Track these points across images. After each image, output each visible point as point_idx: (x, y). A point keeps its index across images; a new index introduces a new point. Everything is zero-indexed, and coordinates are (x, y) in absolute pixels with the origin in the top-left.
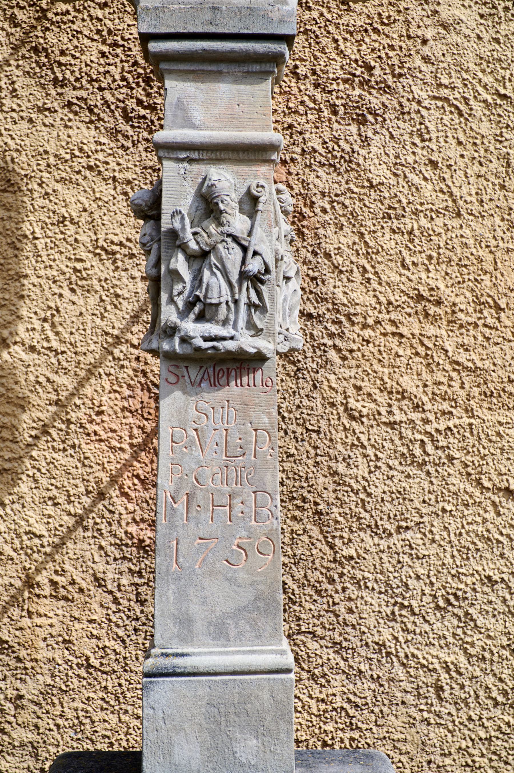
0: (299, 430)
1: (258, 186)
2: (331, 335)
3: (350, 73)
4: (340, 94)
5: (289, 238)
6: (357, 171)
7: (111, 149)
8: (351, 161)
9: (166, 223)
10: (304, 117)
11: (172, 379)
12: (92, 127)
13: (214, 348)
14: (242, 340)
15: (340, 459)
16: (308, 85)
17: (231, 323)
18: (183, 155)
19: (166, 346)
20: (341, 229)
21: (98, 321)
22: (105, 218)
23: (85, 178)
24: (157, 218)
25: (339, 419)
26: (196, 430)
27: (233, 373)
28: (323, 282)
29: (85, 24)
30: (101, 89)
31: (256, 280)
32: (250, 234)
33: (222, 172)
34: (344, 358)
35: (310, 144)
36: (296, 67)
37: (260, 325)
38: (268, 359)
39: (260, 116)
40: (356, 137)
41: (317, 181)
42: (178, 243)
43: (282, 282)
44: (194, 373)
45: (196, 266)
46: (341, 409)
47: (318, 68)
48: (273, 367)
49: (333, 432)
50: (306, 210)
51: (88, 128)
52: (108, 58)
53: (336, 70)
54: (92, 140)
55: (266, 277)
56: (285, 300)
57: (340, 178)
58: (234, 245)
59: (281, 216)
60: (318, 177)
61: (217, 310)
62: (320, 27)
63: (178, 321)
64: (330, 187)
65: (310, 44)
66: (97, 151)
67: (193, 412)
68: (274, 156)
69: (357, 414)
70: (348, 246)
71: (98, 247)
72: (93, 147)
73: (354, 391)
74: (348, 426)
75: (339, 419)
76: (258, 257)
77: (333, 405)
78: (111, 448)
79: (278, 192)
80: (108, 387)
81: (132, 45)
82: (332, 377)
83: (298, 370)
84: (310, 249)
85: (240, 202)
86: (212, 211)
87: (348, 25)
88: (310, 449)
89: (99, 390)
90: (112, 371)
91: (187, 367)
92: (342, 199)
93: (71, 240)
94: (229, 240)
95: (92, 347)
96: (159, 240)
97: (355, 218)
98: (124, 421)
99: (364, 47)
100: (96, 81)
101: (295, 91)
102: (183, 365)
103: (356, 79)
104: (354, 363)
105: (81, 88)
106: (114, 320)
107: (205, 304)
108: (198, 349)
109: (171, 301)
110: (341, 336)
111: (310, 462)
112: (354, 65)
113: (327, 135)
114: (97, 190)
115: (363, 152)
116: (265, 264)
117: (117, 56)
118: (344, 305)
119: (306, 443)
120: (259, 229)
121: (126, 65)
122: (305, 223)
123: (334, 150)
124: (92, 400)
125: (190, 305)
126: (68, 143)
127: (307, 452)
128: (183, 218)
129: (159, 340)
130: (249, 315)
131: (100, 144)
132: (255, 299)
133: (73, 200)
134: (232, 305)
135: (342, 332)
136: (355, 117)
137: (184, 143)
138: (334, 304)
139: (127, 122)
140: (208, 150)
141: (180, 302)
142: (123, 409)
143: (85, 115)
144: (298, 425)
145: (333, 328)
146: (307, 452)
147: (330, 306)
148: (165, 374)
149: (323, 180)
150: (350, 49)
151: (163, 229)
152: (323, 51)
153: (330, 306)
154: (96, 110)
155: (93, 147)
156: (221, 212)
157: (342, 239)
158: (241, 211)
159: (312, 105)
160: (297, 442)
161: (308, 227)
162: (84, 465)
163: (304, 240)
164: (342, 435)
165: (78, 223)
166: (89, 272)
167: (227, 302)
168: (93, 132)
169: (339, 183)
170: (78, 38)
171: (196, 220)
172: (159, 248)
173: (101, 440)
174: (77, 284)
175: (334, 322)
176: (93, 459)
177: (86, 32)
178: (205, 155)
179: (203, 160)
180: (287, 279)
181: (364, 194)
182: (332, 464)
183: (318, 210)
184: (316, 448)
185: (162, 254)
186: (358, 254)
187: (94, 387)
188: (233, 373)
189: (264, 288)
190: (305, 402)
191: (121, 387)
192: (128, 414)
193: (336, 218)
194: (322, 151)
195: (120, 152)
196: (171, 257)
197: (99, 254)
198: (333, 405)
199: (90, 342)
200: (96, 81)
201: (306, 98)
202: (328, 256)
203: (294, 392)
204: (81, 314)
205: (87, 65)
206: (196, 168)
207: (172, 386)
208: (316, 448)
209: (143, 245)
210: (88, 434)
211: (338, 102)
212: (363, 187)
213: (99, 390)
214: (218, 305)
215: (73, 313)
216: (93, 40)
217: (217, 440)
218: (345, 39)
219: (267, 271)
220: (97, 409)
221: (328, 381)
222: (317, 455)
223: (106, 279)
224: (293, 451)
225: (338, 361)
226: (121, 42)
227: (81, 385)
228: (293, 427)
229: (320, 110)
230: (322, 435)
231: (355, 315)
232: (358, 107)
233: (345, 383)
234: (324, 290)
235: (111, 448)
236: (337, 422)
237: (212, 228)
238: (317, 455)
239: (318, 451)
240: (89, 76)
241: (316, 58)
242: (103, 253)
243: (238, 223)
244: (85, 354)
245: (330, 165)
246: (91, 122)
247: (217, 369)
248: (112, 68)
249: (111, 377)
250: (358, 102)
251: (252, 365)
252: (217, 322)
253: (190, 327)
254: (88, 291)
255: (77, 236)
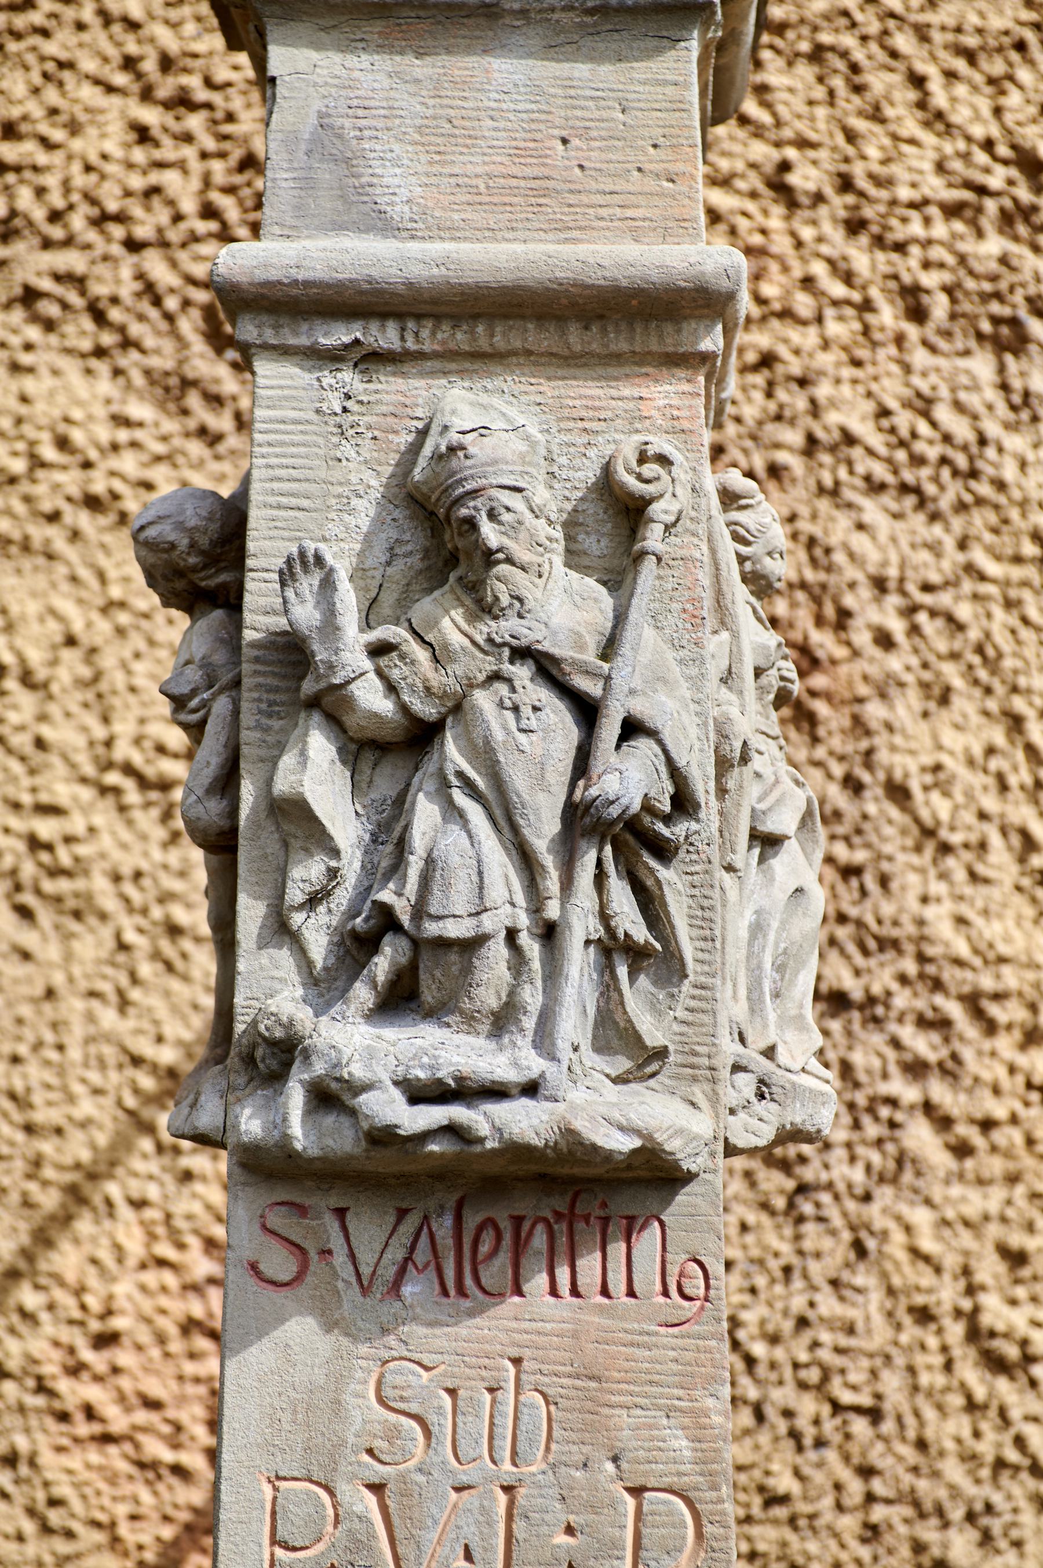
0: (808, 1406)
1: (642, 459)
2: (916, 1069)
3: (968, 185)
4: (937, 253)
5: (771, 679)
6: (997, 507)
7: (164, 439)
8: (974, 474)
9: (262, 609)
10: (813, 331)
11: (279, 1263)
12: (102, 367)
13: (452, 1130)
14: (577, 1095)
15: (957, 1514)
16: (825, 228)
17: (529, 1023)
18: (338, 335)
19: (251, 1124)
20: (945, 699)
21: (108, 1017)
22: (138, 667)
23: (75, 535)
24: (230, 599)
25: (948, 1366)
26: (377, 1488)
27: (539, 1240)
28: (884, 881)
29: (85, 37)
30: (133, 245)
31: (637, 842)
32: (609, 649)
33: (496, 401)
34: (962, 1150)
35: (833, 418)
36: (785, 166)
37: (653, 1035)
38: (690, 1177)
39: (651, 184)
40: (991, 394)
41: (860, 542)
42: (309, 687)
43: (745, 856)
44: (372, 1236)
45: (385, 786)
46: (956, 1331)
47: (858, 170)
48: (711, 1215)
49: (930, 1414)
50: (823, 641)
51: (89, 371)
52: (157, 144)
53: (918, 174)
54: (100, 411)
55: (679, 830)
56: (757, 929)
57: (937, 530)
58: (543, 694)
59: (740, 594)
60: (861, 527)
61: (468, 970)
62: (864, 39)
63: (303, 1016)
64: (903, 565)
65: (831, 93)
66: (115, 447)
67: (364, 1409)
68: (712, 341)
69: (1012, 1352)
70: (971, 762)
71: (108, 766)
72: (104, 433)
73: (1001, 1267)
74: (980, 1393)
75: (948, 1366)
76: (644, 745)
77: (924, 1315)
78: (141, 1465)
79: (729, 498)
80: (135, 1246)
81: (237, 104)
82: (921, 1217)
83: (802, 1189)
84: (838, 770)
85: (571, 526)
86: (452, 560)
87: (959, 30)
88: (846, 1475)
89: (105, 1255)
90: (153, 1192)
91: (341, 1213)
92: (944, 599)
93: (22, 741)
94: (522, 673)
95: (86, 1107)
96: (236, 683)
97: (993, 664)
98: (190, 1368)
99: (1013, 99)
100: (120, 218)
101: (782, 244)
102: (323, 1202)
103: (991, 205)
104: (996, 1166)
105: (69, 242)
106: (162, 1010)
107: (416, 943)
108: (383, 1137)
109: (281, 929)
110: (950, 1070)
111: (849, 1524)
112: (981, 157)
113: (892, 390)
114: (112, 574)
115: (1017, 443)
116: (675, 772)
117: (188, 138)
118: (959, 962)
119: (831, 1456)
120: (649, 633)
121: (217, 167)
122: (819, 681)
123: (914, 435)
124: (79, 1291)
125: (357, 946)
126: (19, 421)
127: (838, 1487)
128: (328, 584)
129: (229, 1096)
130: (609, 988)
131: (121, 421)
132: (630, 922)
133: (33, 608)
134: (532, 948)
135: (955, 1057)
136: (986, 327)
137: (340, 286)
138: (922, 958)
139: (219, 351)
140: (438, 318)
141: (318, 934)
142: (189, 1326)
143: (81, 332)
144: (803, 1386)
145: (923, 1045)
146: (838, 1487)
147: (910, 967)
148: (249, 1242)
149: (880, 537)
150: (968, 106)
151: (249, 635)
152: (876, 115)
153: (910, 967)
154: (115, 315)
155: (104, 433)
156: (489, 557)
157: (949, 737)
158: (574, 558)
159: (838, 290)
160: (800, 1449)
161: (828, 696)
162: (46, 1530)
163: (815, 740)
164: (960, 1425)
165: (45, 685)
166: (82, 850)
167: (511, 935)
168: (105, 386)
169: (934, 548)
170: (61, 84)
171: (388, 599)
172: (236, 712)
173: (107, 1439)
174: (38, 892)
175: (923, 1023)
176: (76, 1505)
177: (89, 65)
178: (427, 338)
179: (420, 356)
180: (768, 843)
181: (1025, 584)
182: (929, 1533)
183: (862, 638)
184: (867, 1472)
185: (245, 735)
186: (1003, 787)
187: (87, 1249)
188: (539, 1240)
189: (669, 877)
190: (828, 1304)
191: (181, 1246)
192: (203, 1343)
193: (925, 666)
194: (877, 441)
195: (196, 448)
196: (281, 748)
197: (116, 791)
198: (924, 1315)
199: (78, 1088)
200: (120, 218)
201: (819, 269)
202: (898, 793)
203: (787, 1270)
204: (50, 994)
205: (88, 168)
206: (391, 388)
207: (279, 1296)
208: (867, 1472)
209: (179, 702)
210: (63, 1417)
211: (930, 279)
212: (1018, 559)
213: (105, 1255)
214: (472, 946)
215: (24, 990)
216: (110, 89)
217: (471, 1533)
218: (950, 75)
219: (683, 803)
220: (95, 1326)
221: (908, 1229)
222: (870, 1498)
223: (138, 875)
224: (784, 1483)
225: (940, 1159)
226: (202, 95)
227: (43, 1238)
228: (784, 1395)
229: (867, 306)
230: (888, 1426)
231: (998, 997)
232: (998, 296)
233: (966, 1239)
234: (888, 909)
235: (141, 1465)
236: (940, 1380)
237: (452, 626)
238: (870, 1498)
239: (878, 1486)
240: (91, 200)
241: (851, 136)
242: (129, 785)
243: (562, 606)
244: (59, 1131)
245: (905, 488)
246: (100, 352)
247: (471, 1221)
248: (170, 179)
249: (150, 1214)
250: (994, 278)
251: (622, 1204)
252: (470, 1020)
253: (355, 1041)
254: (77, 915)
255: (46, 732)
